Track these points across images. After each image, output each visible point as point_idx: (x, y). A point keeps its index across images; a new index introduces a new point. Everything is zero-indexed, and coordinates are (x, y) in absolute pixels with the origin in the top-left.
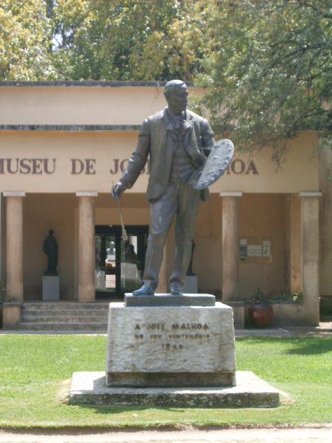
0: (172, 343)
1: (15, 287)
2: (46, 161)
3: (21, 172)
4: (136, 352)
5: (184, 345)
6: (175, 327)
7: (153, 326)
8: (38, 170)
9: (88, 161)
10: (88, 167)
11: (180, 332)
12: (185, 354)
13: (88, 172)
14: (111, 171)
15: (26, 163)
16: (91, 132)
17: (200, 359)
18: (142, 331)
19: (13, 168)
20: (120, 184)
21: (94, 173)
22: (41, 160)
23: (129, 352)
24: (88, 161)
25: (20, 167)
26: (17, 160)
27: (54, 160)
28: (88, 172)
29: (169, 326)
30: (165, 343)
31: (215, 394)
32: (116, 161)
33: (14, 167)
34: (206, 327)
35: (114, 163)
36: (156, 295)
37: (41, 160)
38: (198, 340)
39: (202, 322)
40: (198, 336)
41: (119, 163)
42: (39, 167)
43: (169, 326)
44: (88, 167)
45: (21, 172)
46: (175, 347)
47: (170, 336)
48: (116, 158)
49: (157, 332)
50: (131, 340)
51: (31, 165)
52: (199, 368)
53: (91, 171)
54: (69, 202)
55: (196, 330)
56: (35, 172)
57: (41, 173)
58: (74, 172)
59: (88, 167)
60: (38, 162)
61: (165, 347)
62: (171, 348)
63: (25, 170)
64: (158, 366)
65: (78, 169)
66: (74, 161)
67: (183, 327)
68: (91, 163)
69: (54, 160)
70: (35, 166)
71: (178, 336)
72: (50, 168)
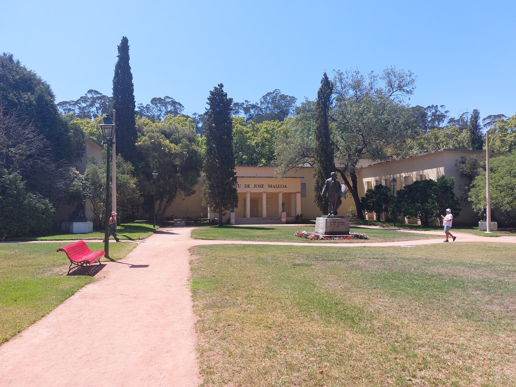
59: (248, 186)
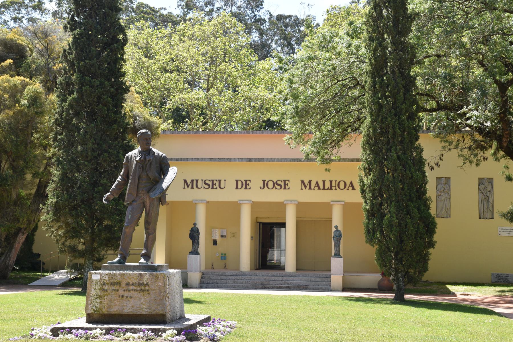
1: (333, 254)
2: (220, 181)
3: (204, 188)
4: (103, 301)
5: (133, 296)
6: (128, 284)
7: (113, 284)
8: (215, 187)
9: (246, 181)
10: (246, 185)
11: (131, 288)
13: (246, 188)
14: (261, 188)
15: (207, 182)
18: (106, 287)
19: (199, 185)
21: (250, 189)
22: (217, 180)
23: (98, 301)
24: (246, 181)
25: (204, 185)
26: (202, 180)
27: (225, 180)
28: (246, 188)
30: (121, 295)
32: (264, 181)
33: (200, 184)
34: (147, 285)
35: (262, 182)
36: (127, 264)
37: (217, 180)
38: (142, 293)
41: (266, 182)
42: (215, 184)
44: (246, 184)
45: (204, 188)
46: (127, 297)
47: (124, 291)
48: (264, 179)
50: (99, 293)
51: (210, 184)
52: (141, 311)
53: (248, 187)
54: (235, 208)
56: (213, 188)
57: (217, 188)
58: (237, 188)
60: (215, 182)
61: (121, 297)
62: (124, 298)
63: (207, 187)
65: (240, 186)
66: (237, 181)
67: (133, 284)
68: (248, 182)
69: (225, 180)
70: (213, 184)
71: (129, 291)
72: (222, 186)
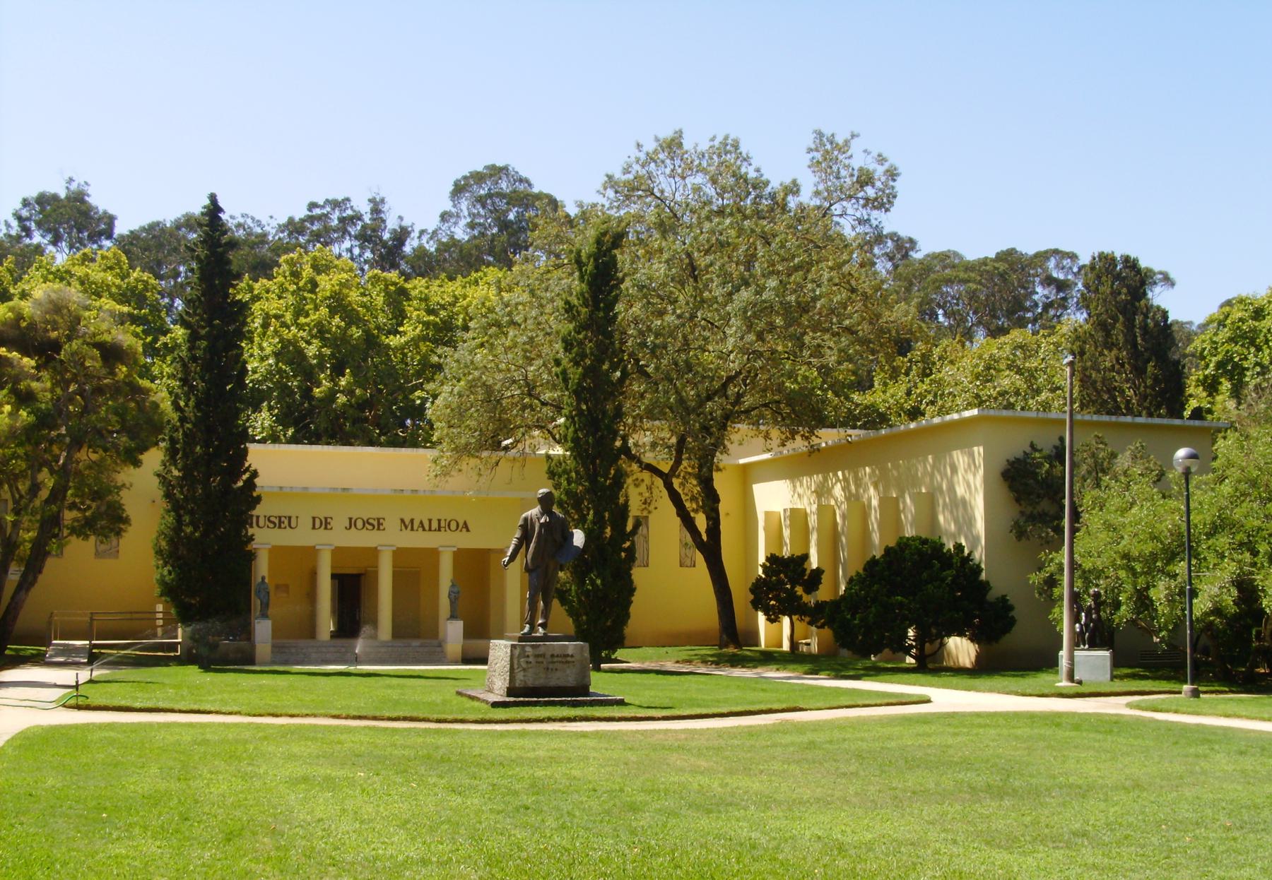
0: (551, 666)
6: (552, 656)
12: (558, 674)
16: (446, 515)
17: (567, 677)
19: (261, 523)
20: (250, 531)
29: (548, 655)
31: (837, 677)
39: (570, 652)
40: (568, 662)
43: (548, 655)
49: (540, 659)
51: (277, 521)
54: (311, 553)
55: (565, 658)
58: (314, 528)
64: (540, 682)
66: (314, 519)
70: (280, 522)
72: (293, 524)
